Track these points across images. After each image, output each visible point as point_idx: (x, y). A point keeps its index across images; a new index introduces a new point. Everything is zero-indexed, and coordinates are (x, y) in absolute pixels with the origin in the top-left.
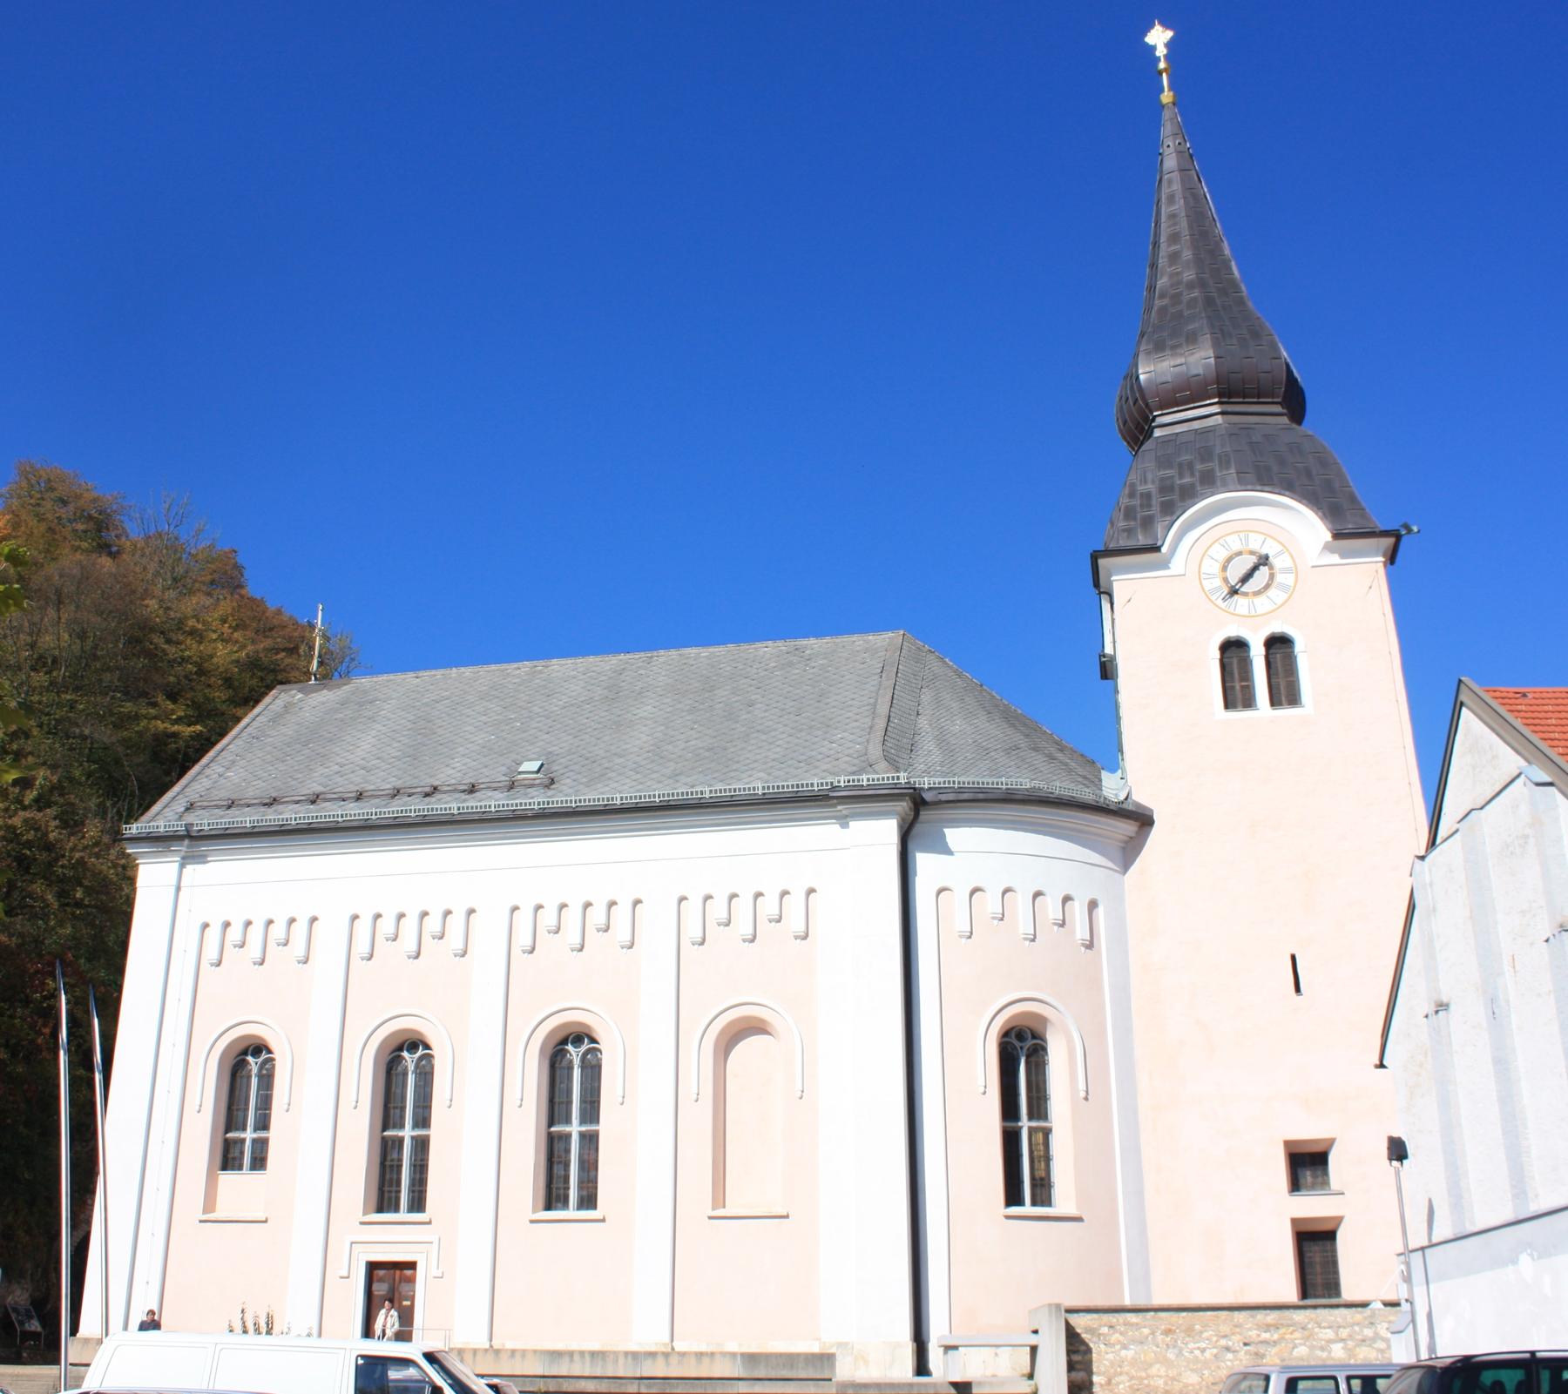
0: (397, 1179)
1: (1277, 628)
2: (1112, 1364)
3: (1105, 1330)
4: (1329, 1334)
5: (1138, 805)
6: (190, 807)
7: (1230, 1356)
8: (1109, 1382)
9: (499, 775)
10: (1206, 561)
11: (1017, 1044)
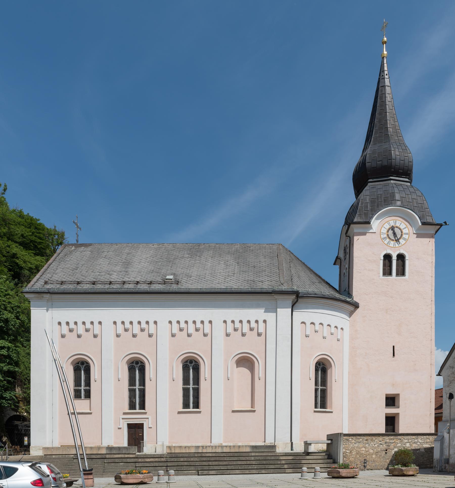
0: (137, 399)
1: (402, 251)
2: (352, 448)
3: (350, 439)
4: (406, 441)
5: (355, 302)
6: (46, 283)
7: (381, 446)
8: (351, 452)
9: (159, 279)
10: (383, 229)
11: (319, 366)
